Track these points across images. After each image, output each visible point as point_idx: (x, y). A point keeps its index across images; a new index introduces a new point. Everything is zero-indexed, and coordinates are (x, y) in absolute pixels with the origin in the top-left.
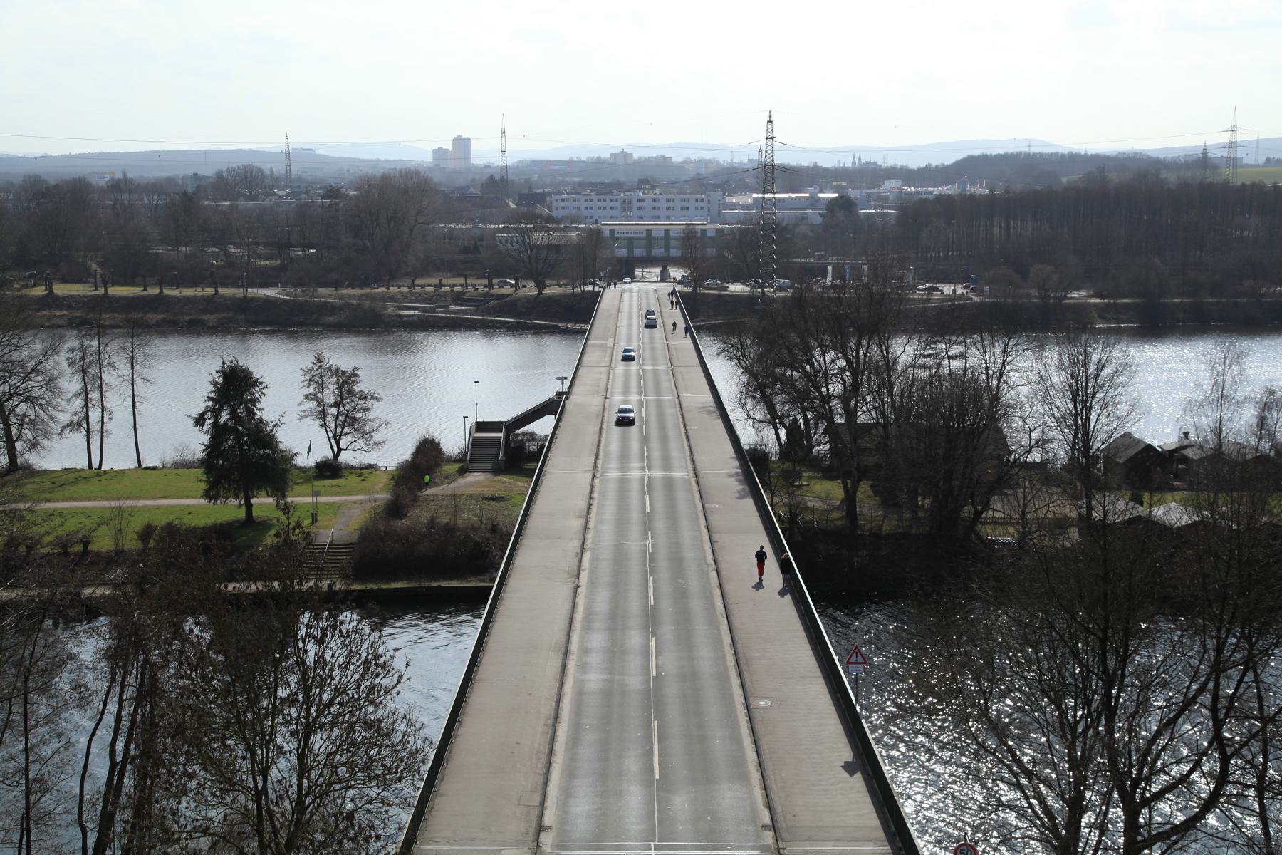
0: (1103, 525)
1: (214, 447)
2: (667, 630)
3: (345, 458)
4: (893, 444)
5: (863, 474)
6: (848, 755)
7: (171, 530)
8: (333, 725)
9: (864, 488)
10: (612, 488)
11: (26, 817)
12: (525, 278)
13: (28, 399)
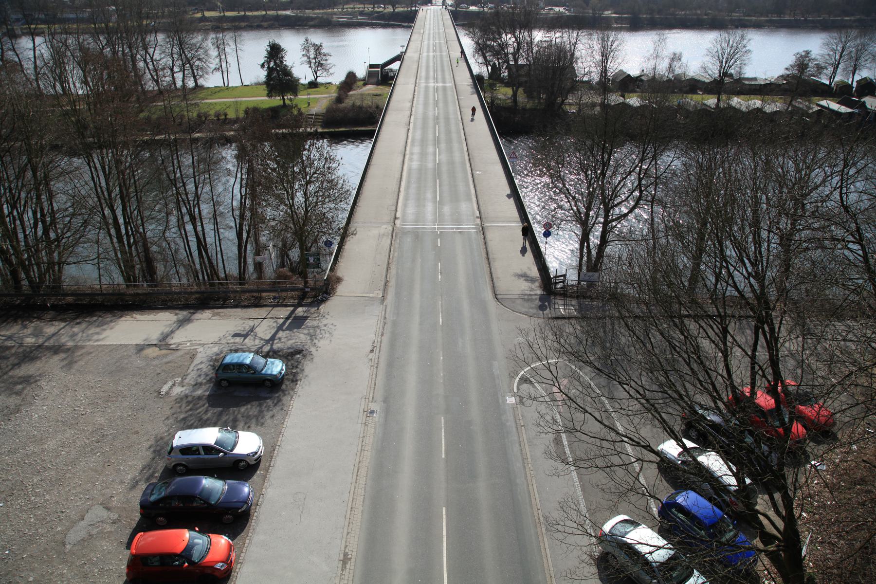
0: (609, 105)
1: (269, 76)
2: (443, 146)
3: (319, 80)
4: (532, 73)
5: (520, 85)
6: (508, 191)
7: (255, 110)
8: (317, 181)
9: (521, 90)
10: (422, 90)
11: (215, 214)
12: (388, 4)
13: (199, 59)
